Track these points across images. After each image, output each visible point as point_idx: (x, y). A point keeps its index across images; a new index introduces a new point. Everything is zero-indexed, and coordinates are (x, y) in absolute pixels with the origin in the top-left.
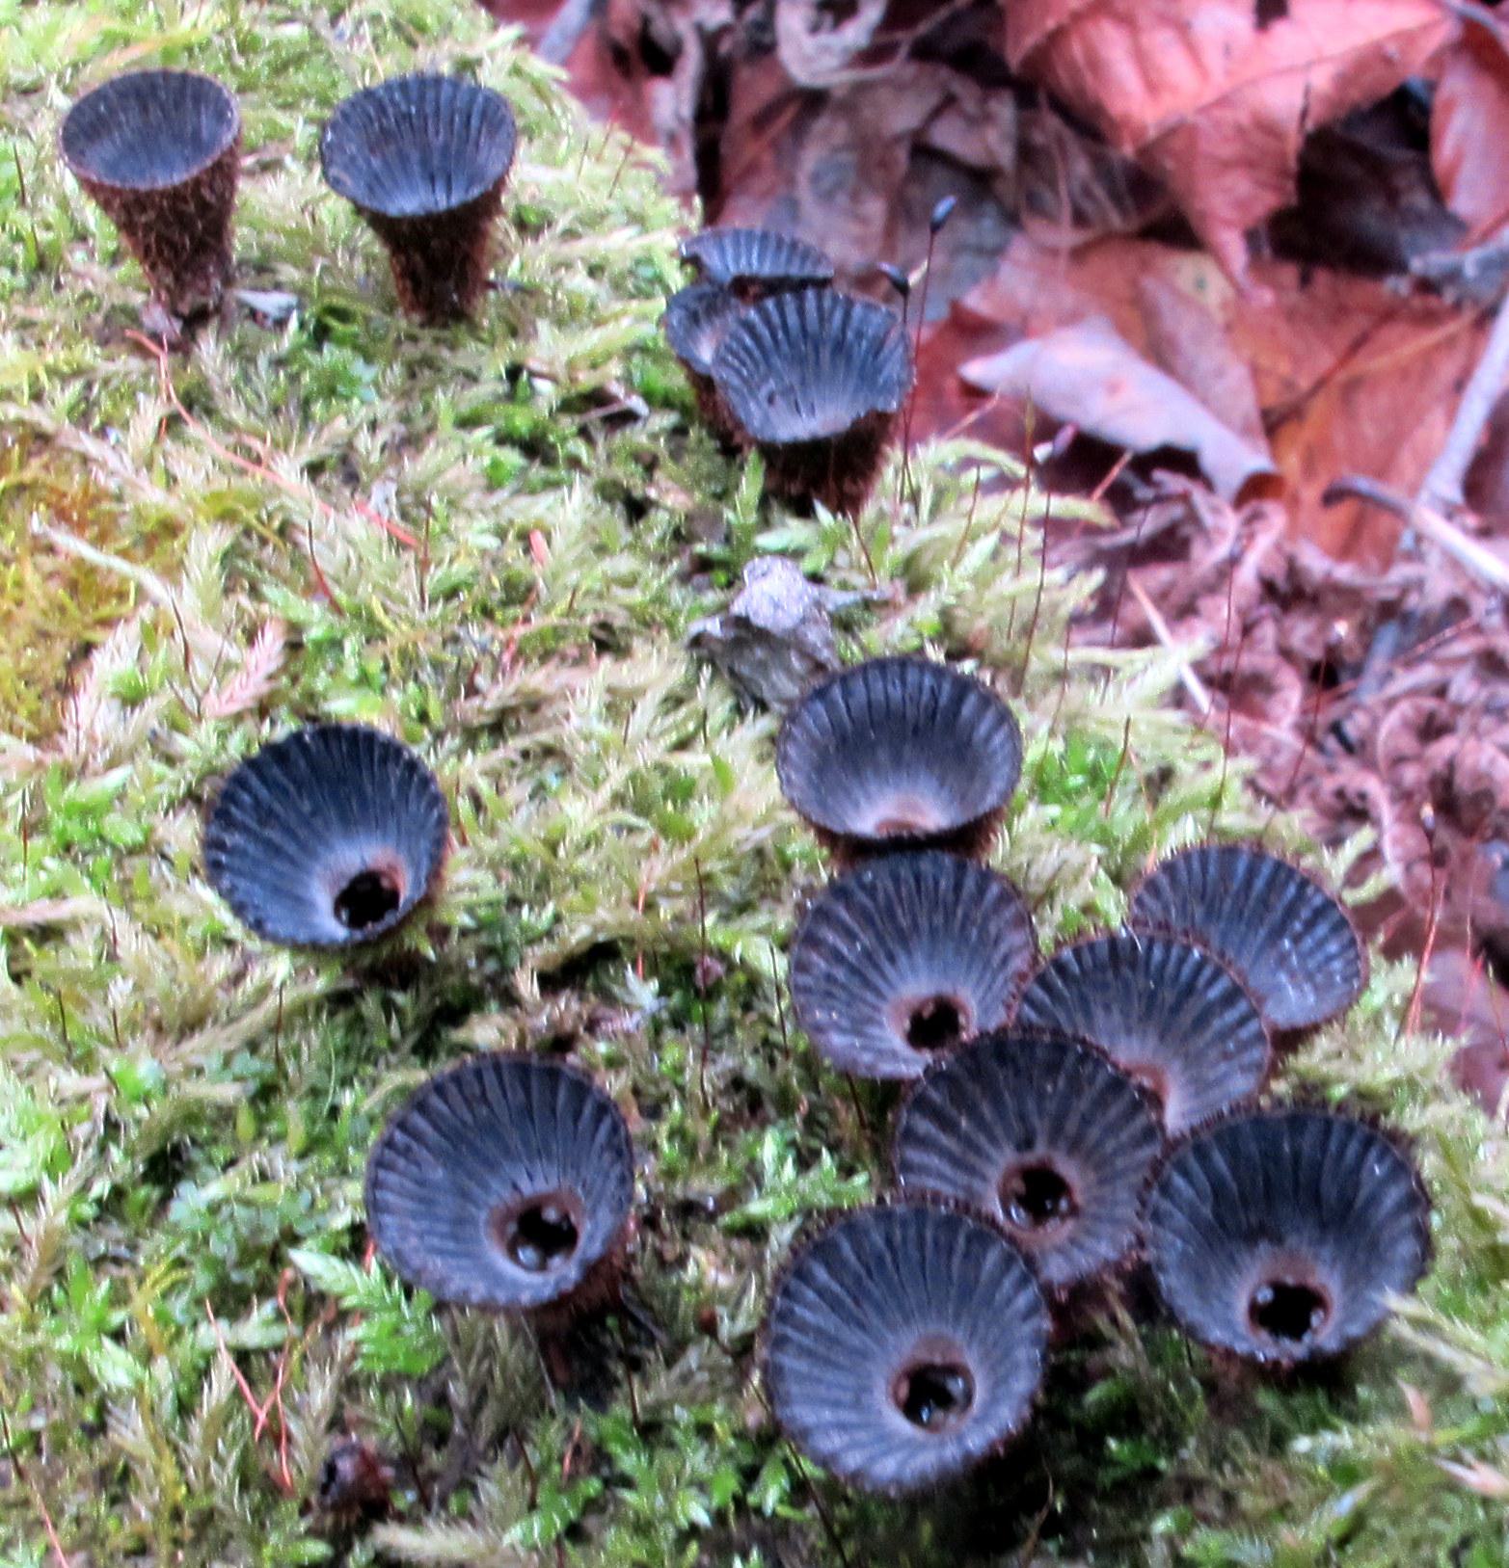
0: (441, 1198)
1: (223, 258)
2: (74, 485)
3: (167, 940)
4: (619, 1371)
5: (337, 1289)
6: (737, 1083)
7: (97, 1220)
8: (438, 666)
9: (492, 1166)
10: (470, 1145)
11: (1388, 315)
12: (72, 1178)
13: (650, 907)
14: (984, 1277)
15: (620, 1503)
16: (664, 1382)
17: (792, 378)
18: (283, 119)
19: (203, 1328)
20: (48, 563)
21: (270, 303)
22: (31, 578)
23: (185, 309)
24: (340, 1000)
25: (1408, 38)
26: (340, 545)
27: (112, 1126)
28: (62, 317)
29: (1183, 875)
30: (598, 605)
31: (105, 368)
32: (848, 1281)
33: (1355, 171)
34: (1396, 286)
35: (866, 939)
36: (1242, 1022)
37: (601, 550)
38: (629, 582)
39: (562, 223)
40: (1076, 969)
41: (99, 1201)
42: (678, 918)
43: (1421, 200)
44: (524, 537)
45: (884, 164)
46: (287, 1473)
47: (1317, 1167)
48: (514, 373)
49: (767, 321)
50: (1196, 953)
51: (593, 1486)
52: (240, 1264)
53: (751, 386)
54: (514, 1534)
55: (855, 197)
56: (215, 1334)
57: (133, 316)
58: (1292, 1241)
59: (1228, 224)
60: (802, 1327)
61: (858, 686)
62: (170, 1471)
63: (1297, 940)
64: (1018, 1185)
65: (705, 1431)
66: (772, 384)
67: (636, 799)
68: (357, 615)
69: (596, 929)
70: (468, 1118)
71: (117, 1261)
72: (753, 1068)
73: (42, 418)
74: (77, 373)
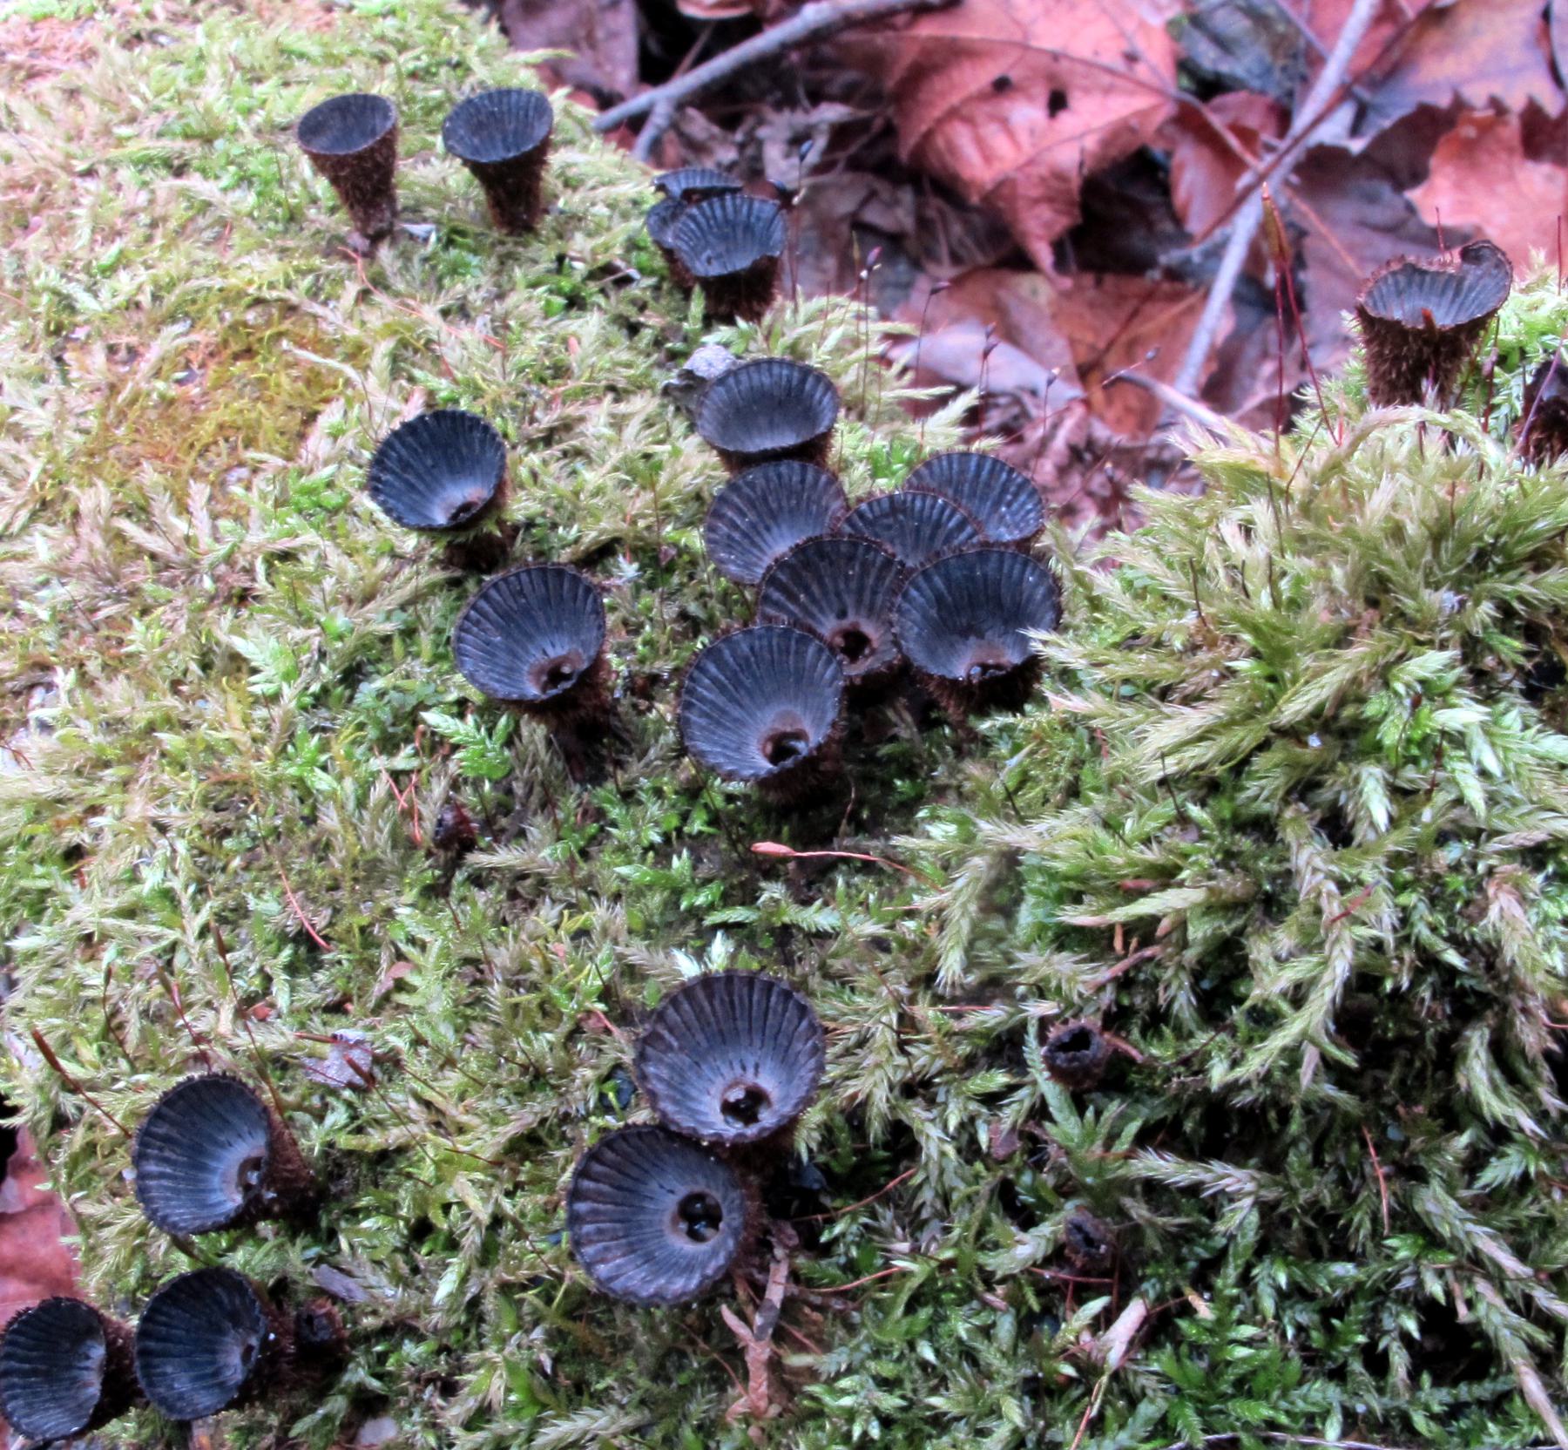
1: (392, 200)
2: (310, 333)
4: (610, 768)
6: (683, 616)
8: (514, 408)
9: (530, 637)
11: (1149, 296)
12: (300, 683)
13: (634, 523)
15: (609, 835)
16: (635, 767)
17: (721, 248)
18: (430, 138)
20: (294, 372)
21: (419, 229)
22: (284, 380)
23: (371, 231)
24: (454, 583)
25: (1143, 114)
27: (323, 655)
28: (304, 244)
29: (936, 469)
31: (327, 268)
33: (1125, 212)
34: (1155, 274)
35: (752, 517)
36: (971, 537)
37: (608, 345)
38: (629, 365)
39: (590, 183)
42: (648, 528)
43: (1168, 227)
44: (565, 341)
45: (834, 236)
46: (418, 833)
48: (561, 259)
51: (593, 828)
53: (697, 253)
54: (546, 852)
55: (818, 257)
56: (379, 763)
57: (342, 240)
58: (989, 634)
59: (1040, 238)
60: (702, 700)
61: (743, 377)
62: (351, 838)
63: (1009, 505)
65: (658, 793)
66: (709, 252)
67: (626, 465)
71: (324, 730)
72: (693, 608)
73: (293, 297)
74: (310, 271)
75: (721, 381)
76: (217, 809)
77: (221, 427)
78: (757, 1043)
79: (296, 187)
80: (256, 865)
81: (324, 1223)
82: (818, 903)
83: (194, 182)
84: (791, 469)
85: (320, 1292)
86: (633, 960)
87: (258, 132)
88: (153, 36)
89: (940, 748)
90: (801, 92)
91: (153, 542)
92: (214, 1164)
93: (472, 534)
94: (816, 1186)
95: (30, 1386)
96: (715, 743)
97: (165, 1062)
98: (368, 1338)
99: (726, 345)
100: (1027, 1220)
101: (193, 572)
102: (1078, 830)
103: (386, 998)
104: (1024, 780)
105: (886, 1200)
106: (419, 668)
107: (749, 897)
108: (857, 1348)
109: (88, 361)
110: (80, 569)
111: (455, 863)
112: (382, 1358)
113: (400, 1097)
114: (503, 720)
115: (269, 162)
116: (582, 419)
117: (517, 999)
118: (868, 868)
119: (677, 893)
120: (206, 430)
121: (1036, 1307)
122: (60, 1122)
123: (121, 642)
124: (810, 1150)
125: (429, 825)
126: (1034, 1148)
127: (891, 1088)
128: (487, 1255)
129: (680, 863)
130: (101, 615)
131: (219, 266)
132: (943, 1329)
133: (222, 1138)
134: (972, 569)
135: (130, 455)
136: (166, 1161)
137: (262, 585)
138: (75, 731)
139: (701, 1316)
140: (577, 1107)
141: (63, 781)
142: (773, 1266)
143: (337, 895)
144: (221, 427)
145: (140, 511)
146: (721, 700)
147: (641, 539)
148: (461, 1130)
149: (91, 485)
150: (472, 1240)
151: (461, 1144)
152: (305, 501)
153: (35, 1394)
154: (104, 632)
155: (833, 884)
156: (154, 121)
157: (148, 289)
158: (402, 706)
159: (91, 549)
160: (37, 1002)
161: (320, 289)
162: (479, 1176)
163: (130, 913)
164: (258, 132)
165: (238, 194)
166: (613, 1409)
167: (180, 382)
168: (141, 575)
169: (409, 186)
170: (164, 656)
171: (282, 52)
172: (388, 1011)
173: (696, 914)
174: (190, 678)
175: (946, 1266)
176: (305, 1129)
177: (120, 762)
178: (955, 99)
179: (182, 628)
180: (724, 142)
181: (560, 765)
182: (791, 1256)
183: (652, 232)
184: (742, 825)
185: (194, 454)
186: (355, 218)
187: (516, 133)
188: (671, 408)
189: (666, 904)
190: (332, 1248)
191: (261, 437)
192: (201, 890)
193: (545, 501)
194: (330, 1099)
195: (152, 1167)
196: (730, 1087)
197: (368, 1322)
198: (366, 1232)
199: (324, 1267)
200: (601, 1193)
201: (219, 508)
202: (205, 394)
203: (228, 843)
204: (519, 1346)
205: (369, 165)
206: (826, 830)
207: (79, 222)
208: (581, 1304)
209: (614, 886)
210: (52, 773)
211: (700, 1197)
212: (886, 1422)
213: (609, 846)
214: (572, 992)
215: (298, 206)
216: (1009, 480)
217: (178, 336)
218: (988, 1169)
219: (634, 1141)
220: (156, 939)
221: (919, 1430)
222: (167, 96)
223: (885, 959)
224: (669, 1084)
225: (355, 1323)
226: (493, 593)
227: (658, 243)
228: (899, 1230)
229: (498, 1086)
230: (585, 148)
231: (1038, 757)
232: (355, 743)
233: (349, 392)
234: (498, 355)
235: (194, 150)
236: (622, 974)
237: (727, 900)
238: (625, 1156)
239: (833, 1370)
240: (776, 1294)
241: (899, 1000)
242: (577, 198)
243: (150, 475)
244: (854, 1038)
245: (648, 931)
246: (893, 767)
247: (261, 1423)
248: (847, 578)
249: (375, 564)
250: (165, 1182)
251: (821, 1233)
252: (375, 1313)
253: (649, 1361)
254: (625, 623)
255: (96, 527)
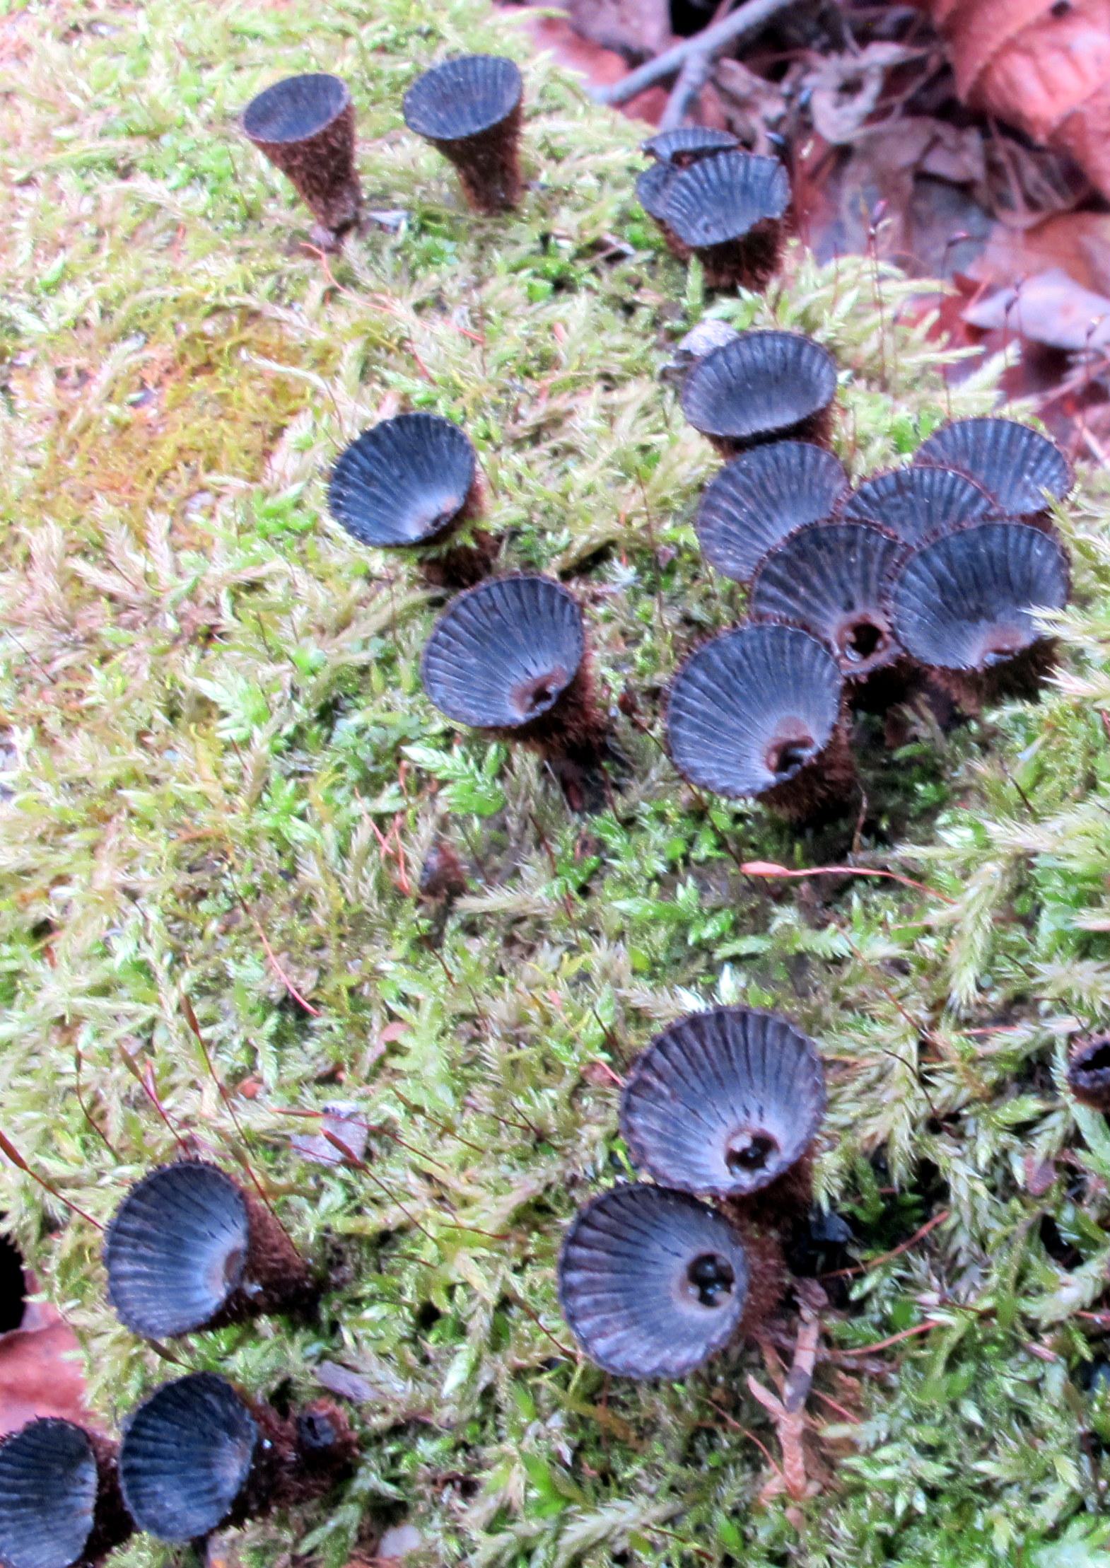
0: (477, 678)
1: (355, 187)
2: (273, 340)
3: (330, 583)
5: (433, 767)
6: (688, 621)
7: (290, 750)
8: (496, 406)
9: (509, 657)
10: (494, 645)
12: (272, 725)
13: (629, 523)
14: (805, 664)
15: (611, 868)
16: (636, 789)
17: (719, 214)
19: (353, 805)
20: (259, 384)
21: (387, 217)
22: (248, 395)
23: (335, 224)
24: (437, 603)
26: (433, 346)
27: (295, 692)
29: (949, 439)
30: (601, 363)
32: (721, 681)
35: (750, 506)
37: (600, 329)
38: (623, 350)
39: (578, 152)
40: (874, 495)
41: (288, 738)
42: (647, 527)
44: (551, 328)
45: (896, 189)
47: (1005, 559)
48: (545, 239)
49: (696, 178)
50: (950, 474)
52: (376, 763)
54: (541, 892)
56: (362, 806)
57: (306, 237)
58: (1001, 617)
60: (692, 711)
61: (733, 354)
62: (335, 891)
63: (1032, 473)
64: (850, 636)
65: (661, 817)
66: (705, 219)
68: (446, 386)
69: (592, 537)
70: (488, 624)
72: (697, 612)
73: (253, 302)
75: (709, 360)
76: (191, 870)
77: (180, 450)
78: (758, 1083)
79: (253, 180)
80: (236, 927)
81: (325, 1316)
82: (833, 926)
83: (140, 183)
84: (788, 450)
85: (327, 1392)
86: (637, 1002)
87: (209, 123)
88: (91, 26)
89: (965, 746)
90: (847, 34)
91: (111, 582)
92: (196, 1259)
93: (444, 548)
94: (841, 1238)
95: (21, 1518)
96: (710, 758)
97: (151, 1151)
98: (377, 1440)
99: (728, 320)
100: (1071, 1258)
101: (155, 612)
102: (1089, 827)
103: (380, 1064)
104: (1041, 775)
105: (922, 1247)
106: (400, 699)
107: (758, 922)
108: (896, 1414)
109: (36, 388)
110: (33, 618)
111: (445, 912)
112: (395, 1460)
113: (398, 1171)
114: (493, 749)
115: (221, 155)
116: (570, 413)
117: (516, 1054)
118: (886, 883)
119: (684, 925)
120: (164, 455)
121: (1088, 1356)
122: (49, 1226)
123: (81, 694)
124: (831, 1199)
125: (416, 870)
126: (1073, 1178)
127: (914, 1127)
128: (497, 1339)
129: (686, 893)
130: (58, 665)
131: (174, 274)
132: (988, 1386)
133: (203, 1229)
134: (974, 546)
135: (84, 488)
136: (143, 1259)
137: (227, 621)
138: (33, 794)
139: (729, 1390)
140: (583, 1169)
141: (23, 851)
142: (801, 1329)
143: (323, 954)
144: (180, 450)
145: (95, 549)
146: (713, 710)
147: (637, 540)
148: (466, 1203)
149: (43, 523)
150: (480, 1323)
151: (465, 1218)
152: (271, 525)
153: (27, 1526)
154: (63, 684)
155: (849, 904)
156: (96, 120)
157: (96, 305)
158: (384, 742)
159: (46, 594)
160: (13, 1095)
161: (283, 291)
162: (484, 1252)
163: (104, 990)
164: (209, 123)
165: (190, 193)
166: (641, 1499)
167: (135, 404)
168: (99, 618)
169: (376, 171)
170: (126, 706)
171: (234, 33)
172: (384, 1077)
173: (704, 947)
174: (155, 728)
175: (985, 1316)
176: (300, 1214)
177: (85, 825)
178: (1011, 30)
179: (145, 674)
180: (769, 94)
181: (556, 794)
182: (820, 1317)
183: (644, 202)
184: (753, 846)
185: (152, 482)
186: (314, 209)
187: (485, 104)
188: (671, 393)
189: (672, 939)
190: (335, 1343)
191: (223, 459)
192: (179, 959)
193: (531, 507)
194: (324, 1179)
195: (125, 1267)
196: (735, 1134)
197: (378, 1422)
198: (372, 1324)
199: (328, 1364)
200: (595, 1261)
201: (181, 539)
202: (163, 415)
203: (204, 906)
204: (538, 1437)
205: (323, 151)
206: (842, 844)
207: (19, 236)
208: (600, 1386)
209: (617, 923)
210: (14, 843)
211: (710, 1259)
212: (933, 1494)
213: (608, 880)
214: (572, 1043)
215: (255, 203)
216: (1031, 445)
217: (130, 354)
218: (1024, 1206)
219: (627, 1201)
220: (131, 1017)
221: (970, 1500)
222: (108, 91)
223: (904, 982)
224: (661, 1136)
225: (364, 1423)
226: (463, 611)
227: (649, 213)
228: (935, 1281)
229: (499, 1152)
230: (573, 115)
231: (1053, 748)
232: (334, 786)
233: (318, 403)
234: (479, 348)
235: (139, 149)
236: (627, 1020)
237: (737, 929)
238: (621, 1219)
239: (871, 1439)
240: (805, 1360)
241: (917, 1026)
242: (561, 169)
243: (104, 509)
244: (874, 1072)
245: (653, 972)
246: (916, 770)
247: (276, 1541)
248: (850, 566)
249: (348, 588)
250: (141, 1283)
251: (851, 1288)
252: (384, 1411)
253: (677, 1444)
254: (624, 634)
255: (49, 569)
